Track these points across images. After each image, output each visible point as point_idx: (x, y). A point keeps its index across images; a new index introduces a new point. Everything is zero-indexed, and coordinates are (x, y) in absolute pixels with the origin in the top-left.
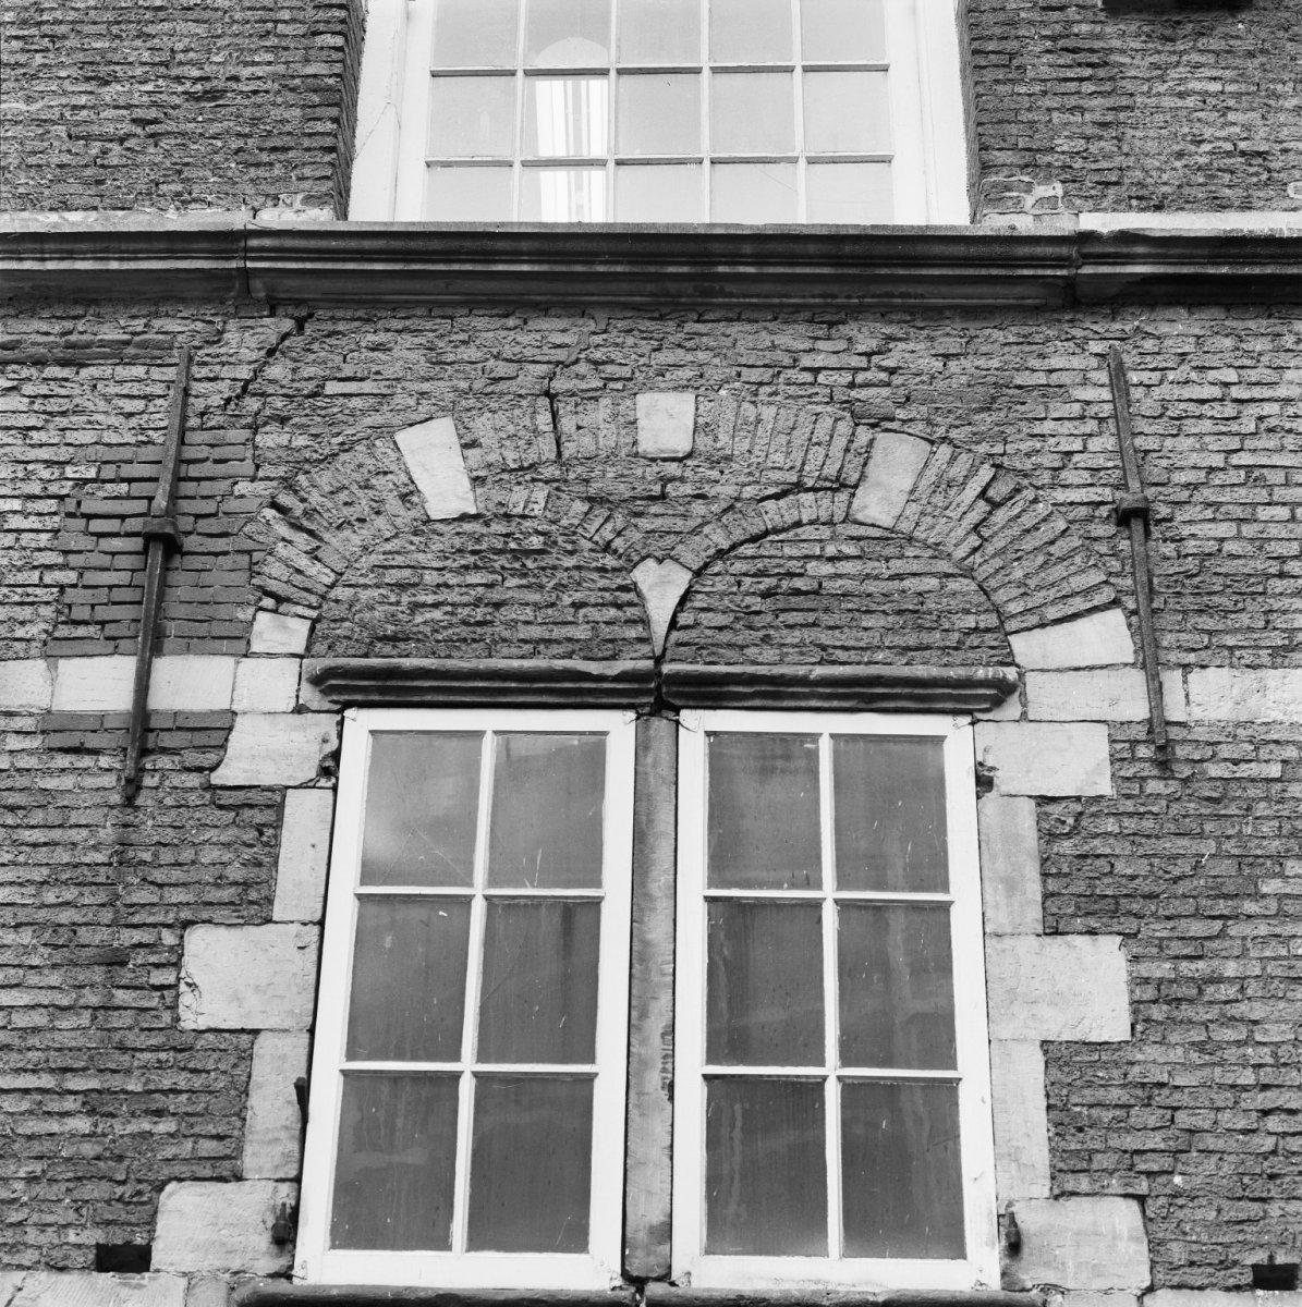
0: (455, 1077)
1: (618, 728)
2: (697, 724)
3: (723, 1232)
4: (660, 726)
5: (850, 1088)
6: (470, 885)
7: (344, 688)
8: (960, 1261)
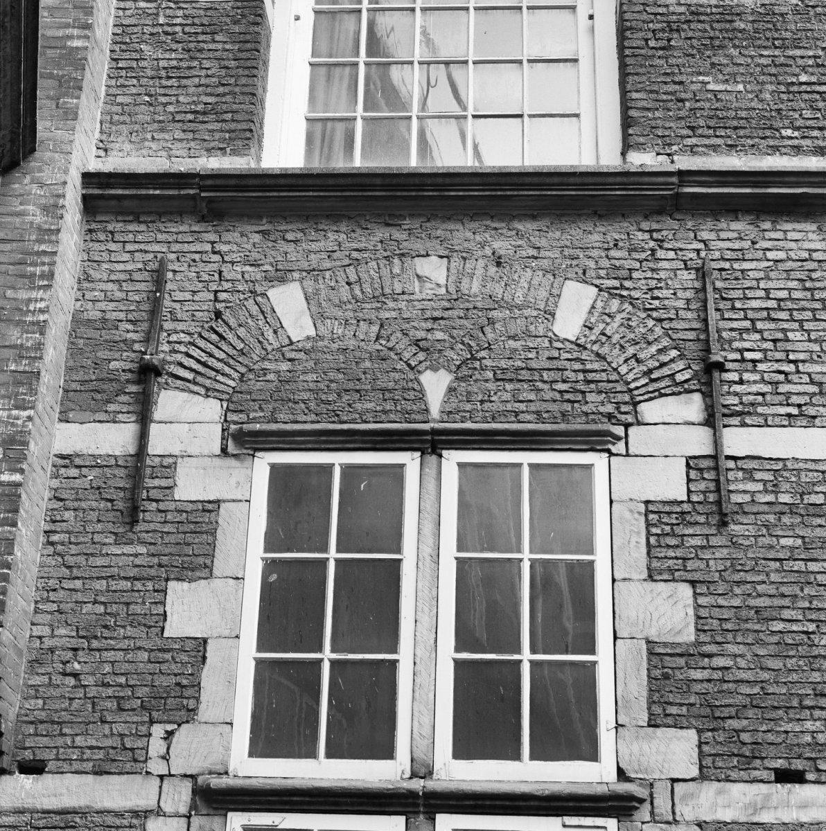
0: (321, 660)
1: (410, 461)
2: (453, 459)
3: (464, 748)
4: (433, 459)
5: (333, 663)
6: (519, 551)
7: (243, 441)
8: (517, 763)
